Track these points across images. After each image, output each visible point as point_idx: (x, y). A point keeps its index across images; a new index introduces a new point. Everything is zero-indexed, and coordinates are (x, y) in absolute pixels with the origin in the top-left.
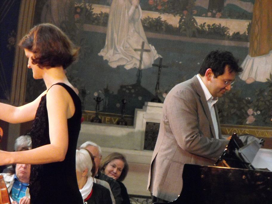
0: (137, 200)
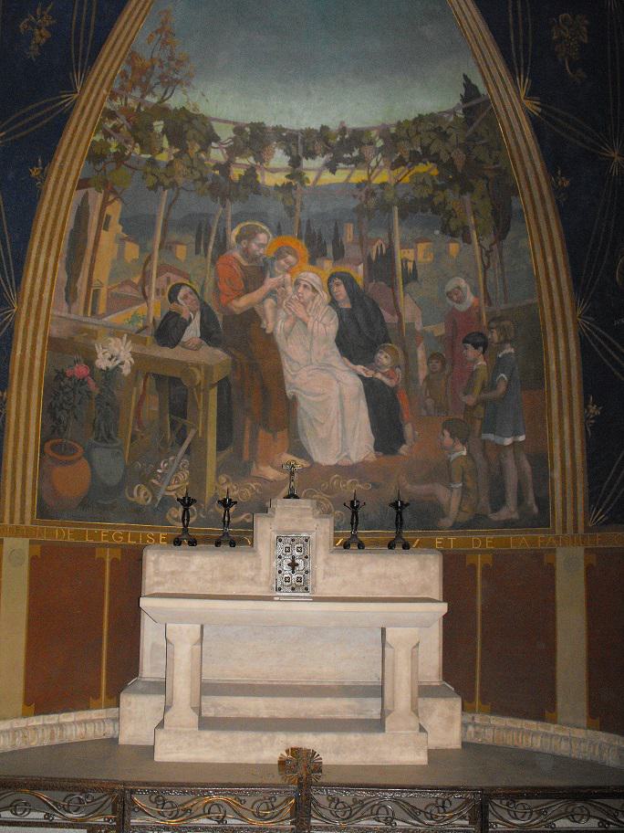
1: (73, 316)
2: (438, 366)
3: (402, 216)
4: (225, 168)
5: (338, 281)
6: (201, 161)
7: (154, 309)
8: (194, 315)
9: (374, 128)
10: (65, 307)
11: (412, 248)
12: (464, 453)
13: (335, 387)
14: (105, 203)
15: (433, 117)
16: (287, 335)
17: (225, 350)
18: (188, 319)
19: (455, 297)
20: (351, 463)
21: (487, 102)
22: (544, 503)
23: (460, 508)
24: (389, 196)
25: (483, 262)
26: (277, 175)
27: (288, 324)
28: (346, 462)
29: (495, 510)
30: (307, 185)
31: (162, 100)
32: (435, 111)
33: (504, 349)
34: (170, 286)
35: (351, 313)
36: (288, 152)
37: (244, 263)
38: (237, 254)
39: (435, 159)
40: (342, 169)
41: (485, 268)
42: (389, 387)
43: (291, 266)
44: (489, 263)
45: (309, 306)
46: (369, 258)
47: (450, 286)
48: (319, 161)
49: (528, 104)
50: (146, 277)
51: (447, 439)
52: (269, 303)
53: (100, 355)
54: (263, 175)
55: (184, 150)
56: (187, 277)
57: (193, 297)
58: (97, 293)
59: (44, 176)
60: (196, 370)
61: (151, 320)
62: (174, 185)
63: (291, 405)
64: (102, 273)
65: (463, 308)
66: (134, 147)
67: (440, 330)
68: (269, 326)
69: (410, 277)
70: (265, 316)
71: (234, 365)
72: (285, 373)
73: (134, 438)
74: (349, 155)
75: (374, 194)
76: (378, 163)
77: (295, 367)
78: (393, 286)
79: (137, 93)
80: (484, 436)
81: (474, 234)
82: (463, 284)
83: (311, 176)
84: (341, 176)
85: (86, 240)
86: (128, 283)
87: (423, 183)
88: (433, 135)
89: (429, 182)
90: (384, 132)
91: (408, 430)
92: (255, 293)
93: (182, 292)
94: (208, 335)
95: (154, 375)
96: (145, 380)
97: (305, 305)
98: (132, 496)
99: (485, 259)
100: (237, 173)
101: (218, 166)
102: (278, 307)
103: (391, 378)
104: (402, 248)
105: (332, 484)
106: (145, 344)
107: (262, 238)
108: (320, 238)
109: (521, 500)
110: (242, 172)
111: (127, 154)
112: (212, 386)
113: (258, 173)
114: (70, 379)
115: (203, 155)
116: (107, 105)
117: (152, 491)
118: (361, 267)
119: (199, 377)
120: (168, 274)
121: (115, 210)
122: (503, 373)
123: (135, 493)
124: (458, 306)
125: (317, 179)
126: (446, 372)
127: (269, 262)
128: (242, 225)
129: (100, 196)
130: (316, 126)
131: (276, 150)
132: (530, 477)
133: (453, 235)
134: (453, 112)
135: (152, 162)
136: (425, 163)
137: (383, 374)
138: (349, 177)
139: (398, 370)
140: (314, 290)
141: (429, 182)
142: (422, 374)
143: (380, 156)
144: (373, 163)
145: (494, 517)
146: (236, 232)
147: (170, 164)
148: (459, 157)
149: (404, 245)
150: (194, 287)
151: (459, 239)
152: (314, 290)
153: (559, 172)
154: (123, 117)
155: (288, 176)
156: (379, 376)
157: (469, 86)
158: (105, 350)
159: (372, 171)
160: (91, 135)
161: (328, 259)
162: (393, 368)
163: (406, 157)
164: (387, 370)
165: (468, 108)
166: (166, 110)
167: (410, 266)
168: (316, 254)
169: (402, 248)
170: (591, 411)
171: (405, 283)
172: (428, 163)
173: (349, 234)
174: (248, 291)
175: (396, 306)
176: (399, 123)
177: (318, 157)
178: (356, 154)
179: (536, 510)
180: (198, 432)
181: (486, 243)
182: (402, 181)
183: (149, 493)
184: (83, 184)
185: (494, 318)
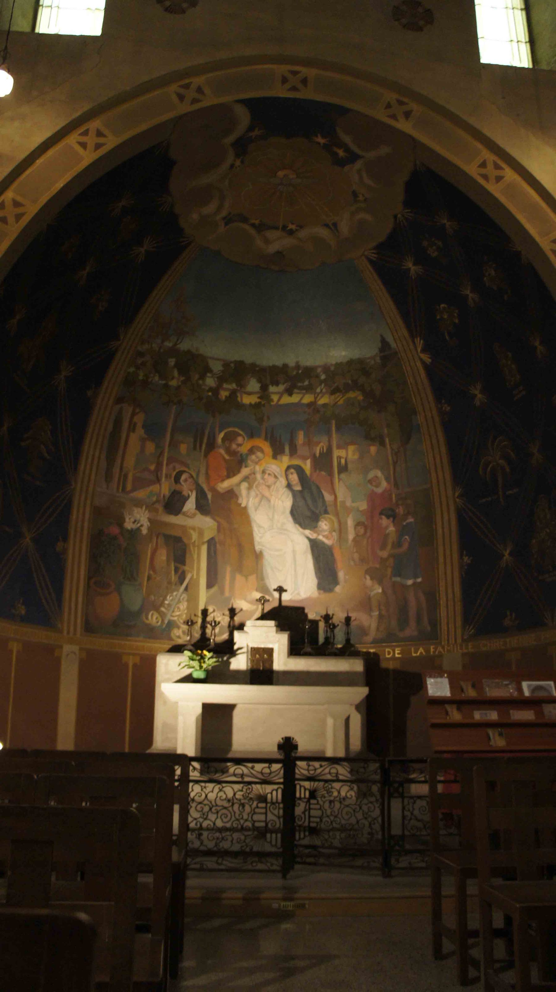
0: (253, 768)
2: (362, 531)
3: (338, 428)
4: (215, 391)
5: (292, 470)
12: (380, 590)
14: (133, 414)
15: (361, 361)
18: (187, 495)
21: (396, 353)
22: (434, 623)
27: (257, 500)
30: (272, 403)
31: (176, 344)
34: (175, 473)
36: (260, 381)
39: (361, 388)
42: (327, 545)
43: (260, 460)
46: (314, 455)
47: (371, 475)
48: (281, 388)
50: (159, 466)
51: (368, 582)
52: (244, 485)
53: (127, 520)
57: (190, 480)
58: (126, 476)
60: (192, 532)
61: (162, 495)
64: (130, 461)
65: (379, 490)
75: (318, 411)
76: (321, 390)
78: (331, 474)
80: (394, 579)
81: (387, 440)
82: (379, 474)
83: (275, 398)
84: (295, 399)
91: (341, 575)
93: (184, 477)
98: (147, 618)
100: (224, 394)
101: (211, 389)
102: (249, 488)
107: (240, 440)
110: (227, 393)
112: (203, 543)
113: (239, 395)
116: (139, 348)
117: (161, 616)
118: (308, 462)
119: (194, 536)
121: (139, 419)
123: (150, 617)
125: (279, 400)
129: (131, 409)
135: (166, 386)
137: (324, 536)
138: (301, 399)
139: (334, 534)
140: (276, 477)
142: (351, 536)
143: (323, 385)
146: (222, 435)
147: (178, 388)
149: (339, 447)
152: (276, 477)
155: (259, 398)
156: (321, 537)
157: (384, 341)
159: (318, 395)
162: (330, 532)
164: (326, 533)
167: (343, 461)
171: (339, 473)
174: (228, 477)
178: (306, 383)
179: (429, 628)
180: (193, 575)
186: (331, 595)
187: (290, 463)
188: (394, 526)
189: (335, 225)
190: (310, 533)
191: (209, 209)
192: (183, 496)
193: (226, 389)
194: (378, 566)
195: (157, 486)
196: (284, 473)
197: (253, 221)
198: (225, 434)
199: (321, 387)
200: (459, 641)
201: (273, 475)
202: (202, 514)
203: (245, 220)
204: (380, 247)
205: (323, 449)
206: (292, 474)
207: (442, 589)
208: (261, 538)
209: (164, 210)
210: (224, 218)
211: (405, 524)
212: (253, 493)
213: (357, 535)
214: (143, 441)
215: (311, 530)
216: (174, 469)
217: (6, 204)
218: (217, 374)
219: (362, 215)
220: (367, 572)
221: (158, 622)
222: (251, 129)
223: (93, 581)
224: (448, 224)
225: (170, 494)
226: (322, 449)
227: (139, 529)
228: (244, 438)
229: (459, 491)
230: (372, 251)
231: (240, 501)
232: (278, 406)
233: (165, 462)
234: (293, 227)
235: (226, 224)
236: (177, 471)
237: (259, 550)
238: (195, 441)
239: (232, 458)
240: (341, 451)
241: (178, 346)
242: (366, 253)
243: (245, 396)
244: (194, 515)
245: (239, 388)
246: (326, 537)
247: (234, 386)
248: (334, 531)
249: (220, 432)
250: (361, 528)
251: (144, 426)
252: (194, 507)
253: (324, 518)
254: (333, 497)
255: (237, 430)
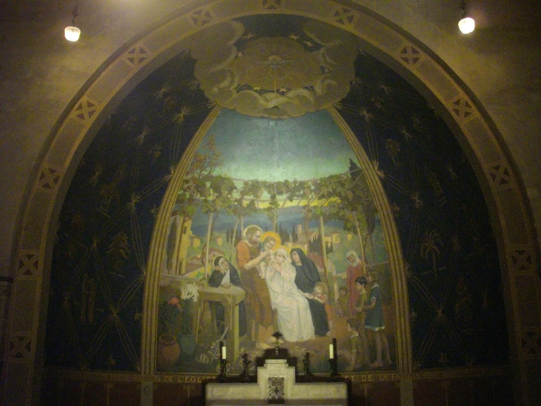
1: (170, 275)
2: (344, 293)
3: (325, 222)
4: (240, 201)
5: (295, 252)
6: (228, 198)
7: (208, 269)
8: (227, 271)
9: (310, 181)
10: (167, 271)
11: (330, 236)
12: (357, 335)
13: (295, 303)
14: (184, 221)
15: (337, 177)
16: (272, 280)
17: (243, 288)
18: (223, 273)
19: (351, 260)
20: (304, 341)
21: (360, 171)
22: (394, 358)
23: (356, 362)
24: (318, 212)
25: (363, 243)
26: (265, 203)
27: (272, 274)
28: (301, 340)
29: (372, 363)
30: (279, 207)
31: (210, 173)
32: (338, 174)
33: (374, 285)
34: (215, 258)
35: (302, 267)
36: (269, 192)
37: (250, 245)
38: (247, 241)
39: (339, 195)
40: (295, 199)
41: (364, 247)
42: (321, 303)
43: (273, 246)
44: (366, 244)
45: (282, 265)
46: (310, 241)
47: (349, 254)
48: (285, 196)
49: (379, 173)
50: (204, 254)
51: (349, 329)
52: (263, 264)
53: (183, 293)
54: (258, 203)
55: (220, 194)
56: (223, 253)
57: (226, 263)
58: (181, 264)
59: (157, 212)
60: (228, 298)
61: (207, 274)
62: (215, 210)
63: (274, 313)
64: (183, 253)
65: (354, 265)
66: (197, 194)
67: (344, 276)
68: (262, 275)
69: (330, 250)
70: (261, 271)
71: (247, 294)
72: (271, 297)
73: (200, 332)
74: (298, 193)
75: (311, 211)
76: (312, 197)
77: (276, 294)
78: (321, 254)
79: (199, 171)
80: (366, 327)
81: (359, 230)
82: (355, 254)
83: (281, 203)
84: (295, 203)
85: (175, 239)
86: (196, 258)
87: (334, 206)
88: (337, 184)
89: (336, 205)
90: (315, 183)
91: (331, 324)
92: (256, 259)
93: (221, 261)
94: (234, 281)
95: (209, 301)
96: (204, 304)
97: (280, 264)
98: (199, 360)
99: (364, 241)
100: (245, 203)
101: (236, 200)
102: (267, 265)
103: (323, 299)
104: (325, 236)
105: (295, 351)
106: (204, 287)
107: (258, 233)
108: (286, 232)
109: (384, 358)
110: (248, 202)
111: (194, 198)
112: (236, 305)
113: (256, 203)
114: (170, 305)
115: (229, 196)
116: (185, 178)
117: (209, 357)
118: (306, 246)
119: (230, 300)
120: (214, 252)
121: (189, 224)
122: (374, 296)
123: (201, 358)
124: (352, 264)
125: (284, 204)
126: (348, 296)
127: (262, 244)
128: (249, 227)
129: (182, 218)
130: (282, 180)
131: (264, 191)
132: (387, 346)
133: (349, 230)
134: (346, 174)
135: (206, 201)
136: (334, 197)
137: (318, 297)
138: (299, 203)
139: (325, 295)
140: (284, 257)
141: (336, 205)
142: (337, 296)
143: (313, 193)
144: (310, 197)
145: (371, 366)
146: (246, 230)
147: (214, 201)
148: (350, 195)
149: (326, 235)
150: (227, 258)
151: (352, 232)
152: (284, 257)
153: (395, 204)
154: (192, 182)
155: (270, 204)
156: (316, 298)
157: (352, 163)
158: (185, 290)
159: (310, 200)
160: (178, 191)
161: (290, 242)
162: (322, 294)
163: (326, 194)
164: (320, 295)
165: (353, 173)
166: (212, 177)
167: (329, 245)
168: (284, 239)
169: (325, 236)
170: (413, 315)
171: (327, 253)
172: (336, 197)
173: (300, 230)
174: (252, 259)
175: (323, 264)
176: (321, 179)
177: (284, 194)
178: (302, 192)
179: (390, 362)
180: (230, 327)
181: (364, 234)
182: (324, 206)
183: (207, 358)
184: (174, 213)
185: (369, 270)
186: (324, 338)
187: (294, 247)
188: (366, 290)
189: (312, 87)
190: (309, 295)
191: (225, 83)
192: (222, 273)
193: (247, 200)
194: (355, 317)
195: (203, 268)
196: (289, 254)
197: (255, 88)
198: (248, 230)
199: (312, 195)
200: (410, 371)
201: (282, 256)
202: (234, 285)
203: (250, 88)
204: (343, 101)
205: (316, 237)
206: (295, 254)
207: (399, 334)
208: (275, 299)
209: (193, 89)
210: (235, 88)
211: (372, 288)
212: (269, 269)
213: (341, 296)
214: (192, 238)
215: (309, 293)
216: (214, 256)
217: (83, 105)
218: (239, 190)
219: (328, 81)
220: (349, 321)
221: (206, 361)
222: (245, 34)
223: (160, 337)
224: (386, 88)
225: (212, 273)
226: (314, 237)
227: (191, 299)
228: (261, 231)
229: (408, 266)
230: (339, 104)
231: (260, 275)
232: (283, 209)
233: (207, 253)
234: (284, 90)
235: (238, 92)
236: (216, 257)
237: (275, 308)
238: (228, 238)
239: (253, 246)
240: (327, 238)
241: (212, 173)
242: (335, 105)
243: (260, 203)
244: (229, 287)
245: (256, 198)
246: (320, 298)
247: (252, 197)
248: (325, 293)
249: (244, 228)
250: (343, 291)
251: (192, 229)
252: (229, 280)
253: (318, 284)
254: (324, 270)
255: (256, 226)
